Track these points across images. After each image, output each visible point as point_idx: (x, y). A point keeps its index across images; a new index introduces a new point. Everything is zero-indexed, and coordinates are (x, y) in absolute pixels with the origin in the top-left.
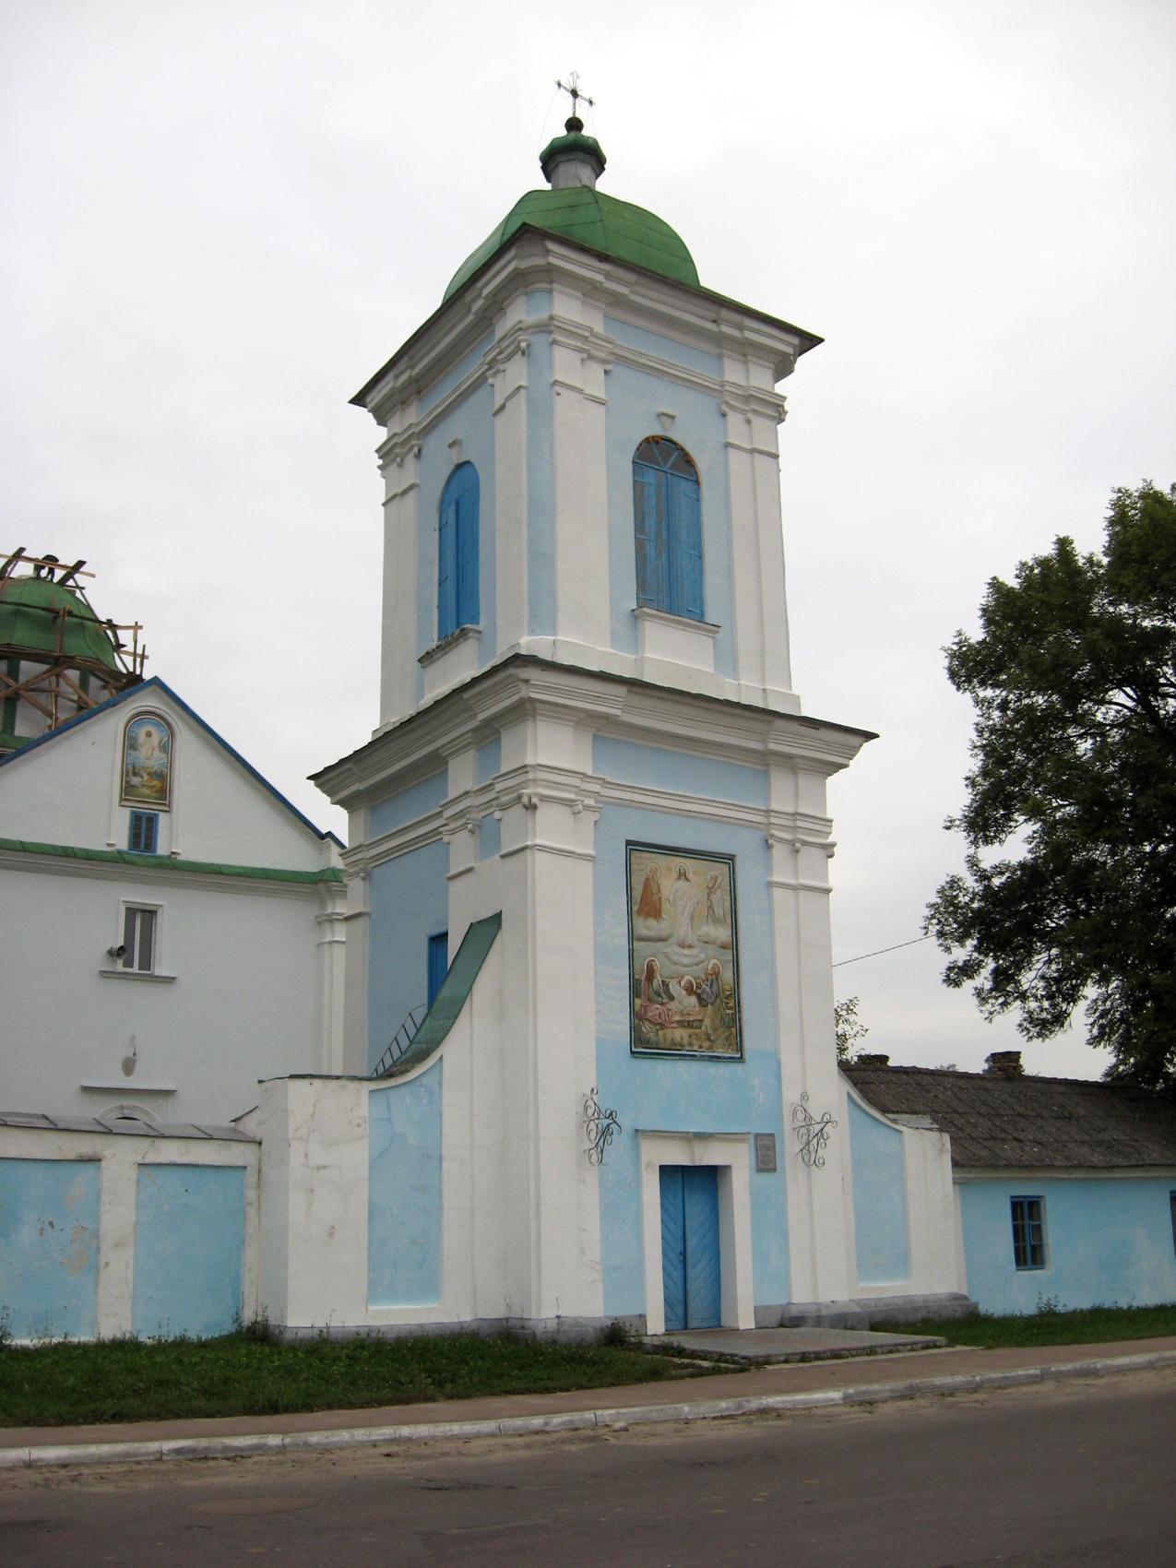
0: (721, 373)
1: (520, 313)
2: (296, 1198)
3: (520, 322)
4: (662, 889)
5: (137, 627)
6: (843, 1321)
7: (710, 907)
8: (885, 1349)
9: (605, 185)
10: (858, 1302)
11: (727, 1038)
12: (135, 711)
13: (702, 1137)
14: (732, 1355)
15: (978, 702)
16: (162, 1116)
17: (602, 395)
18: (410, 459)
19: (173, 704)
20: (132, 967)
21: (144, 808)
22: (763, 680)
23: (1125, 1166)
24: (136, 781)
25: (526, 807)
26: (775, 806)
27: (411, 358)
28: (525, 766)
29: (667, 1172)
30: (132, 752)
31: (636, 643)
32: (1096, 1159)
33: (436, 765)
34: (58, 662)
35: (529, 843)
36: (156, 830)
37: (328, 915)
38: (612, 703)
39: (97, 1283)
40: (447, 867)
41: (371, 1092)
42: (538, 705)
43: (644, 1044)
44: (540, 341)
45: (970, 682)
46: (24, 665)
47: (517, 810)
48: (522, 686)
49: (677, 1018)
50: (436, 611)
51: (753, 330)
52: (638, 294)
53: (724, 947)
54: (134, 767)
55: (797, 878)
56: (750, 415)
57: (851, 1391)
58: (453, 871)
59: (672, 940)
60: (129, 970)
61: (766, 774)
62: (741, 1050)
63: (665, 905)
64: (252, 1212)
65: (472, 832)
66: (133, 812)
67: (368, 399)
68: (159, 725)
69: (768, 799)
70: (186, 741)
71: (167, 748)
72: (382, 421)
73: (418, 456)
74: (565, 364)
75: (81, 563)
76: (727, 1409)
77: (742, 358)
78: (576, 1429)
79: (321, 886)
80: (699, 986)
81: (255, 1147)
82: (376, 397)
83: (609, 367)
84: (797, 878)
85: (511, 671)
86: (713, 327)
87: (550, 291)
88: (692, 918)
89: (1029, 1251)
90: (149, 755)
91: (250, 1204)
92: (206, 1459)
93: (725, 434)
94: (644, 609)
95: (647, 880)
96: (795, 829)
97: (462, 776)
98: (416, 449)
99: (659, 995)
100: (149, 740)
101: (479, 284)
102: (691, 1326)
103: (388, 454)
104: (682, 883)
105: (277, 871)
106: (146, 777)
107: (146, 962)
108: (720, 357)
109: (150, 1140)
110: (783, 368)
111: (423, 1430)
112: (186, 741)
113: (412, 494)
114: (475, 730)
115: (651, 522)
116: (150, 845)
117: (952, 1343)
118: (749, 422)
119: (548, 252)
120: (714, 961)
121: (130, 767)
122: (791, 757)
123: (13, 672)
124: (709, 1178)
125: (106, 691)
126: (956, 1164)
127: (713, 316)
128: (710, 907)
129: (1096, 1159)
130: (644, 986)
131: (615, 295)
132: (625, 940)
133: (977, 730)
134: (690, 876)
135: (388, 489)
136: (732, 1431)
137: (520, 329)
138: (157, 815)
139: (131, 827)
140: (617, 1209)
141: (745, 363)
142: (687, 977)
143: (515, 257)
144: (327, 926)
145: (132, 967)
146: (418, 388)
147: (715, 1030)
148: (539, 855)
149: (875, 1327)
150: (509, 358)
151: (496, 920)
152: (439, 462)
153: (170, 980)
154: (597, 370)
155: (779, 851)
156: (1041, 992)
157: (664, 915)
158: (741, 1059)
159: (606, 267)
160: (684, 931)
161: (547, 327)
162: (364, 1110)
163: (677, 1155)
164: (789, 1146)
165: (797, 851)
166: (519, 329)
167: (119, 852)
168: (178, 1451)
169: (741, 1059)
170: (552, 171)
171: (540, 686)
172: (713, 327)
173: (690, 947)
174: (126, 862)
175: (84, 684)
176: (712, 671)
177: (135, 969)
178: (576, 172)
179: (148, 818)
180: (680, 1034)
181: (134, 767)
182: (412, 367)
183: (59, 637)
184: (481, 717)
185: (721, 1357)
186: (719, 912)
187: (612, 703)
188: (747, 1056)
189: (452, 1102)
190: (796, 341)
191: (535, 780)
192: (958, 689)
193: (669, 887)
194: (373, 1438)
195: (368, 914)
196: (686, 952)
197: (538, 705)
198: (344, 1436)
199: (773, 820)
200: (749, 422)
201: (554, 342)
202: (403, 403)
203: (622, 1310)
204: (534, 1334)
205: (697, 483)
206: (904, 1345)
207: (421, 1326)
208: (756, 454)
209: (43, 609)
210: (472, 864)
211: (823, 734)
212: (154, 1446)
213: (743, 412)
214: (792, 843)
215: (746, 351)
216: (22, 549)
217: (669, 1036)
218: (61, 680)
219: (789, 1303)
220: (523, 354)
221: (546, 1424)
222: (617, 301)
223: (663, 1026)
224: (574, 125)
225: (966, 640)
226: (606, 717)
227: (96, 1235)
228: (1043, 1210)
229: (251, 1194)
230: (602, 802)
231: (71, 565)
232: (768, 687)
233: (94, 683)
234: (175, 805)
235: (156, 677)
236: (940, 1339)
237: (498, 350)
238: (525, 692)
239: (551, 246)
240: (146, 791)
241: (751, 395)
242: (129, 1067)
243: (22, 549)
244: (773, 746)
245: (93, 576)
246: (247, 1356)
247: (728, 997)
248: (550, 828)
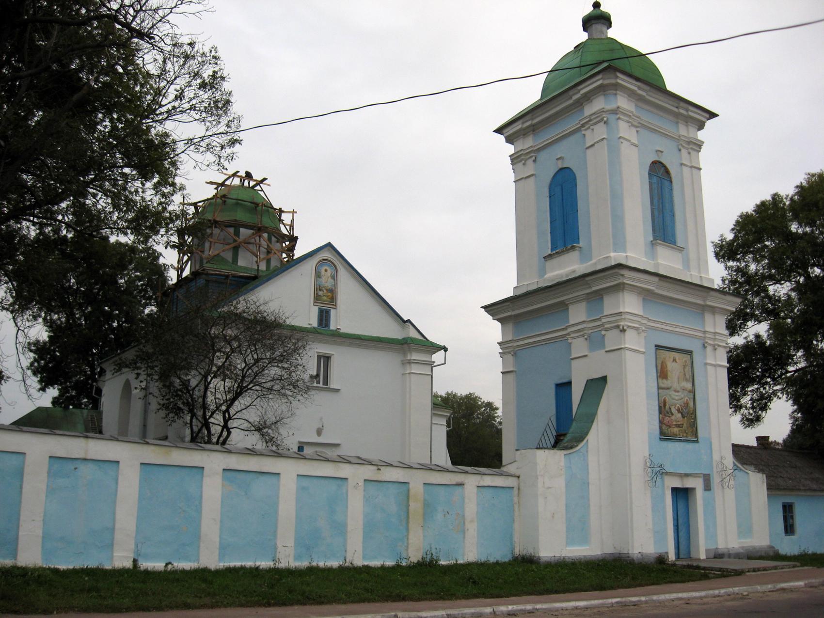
0: (678, 130)
1: (598, 104)
2: (541, 500)
3: (603, 108)
4: (668, 366)
5: (294, 212)
6: (738, 556)
7: (685, 374)
8: (780, 567)
9: (611, 33)
10: (743, 548)
11: (692, 432)
12: (320, 259)
13: (687, 475)
14: (727, 569)
15: (726, 268)
16: (330, 453)
17: (636, 142)
18: (530, 161)
19: (337, 256)
20: (319, 384)
21: (325, 307)
22: (699, 272)
24: (320, 293)
25: (621, 331)
26: (707, 329)
27: (533, 115)
28: (621, 313)
30: (318, 279)
31: (653, 255)
32: (815, 487)
33: (563, 307)
34: (259, 230)
35: (623, 346)
36: (330, 317)
37: (409, 360)
38: (651, 284)
39: (464, 538)
40: (570, 354)
41: (565, 455)
42: (626, 286)
43: (665, 435)
44: (612, 118)
45: (724, 258)
46: (242, 230)
47: (616, 332)
48: (620, 277)
49: (674, 423)
50: (549, 235)
51: (692, 111)
53: (690, 392)
54: (320, 287)
55: (716, 361)
56: (690, 150)
57: (807, 582)
58: (572, 357)
59: (672, 388)
60: (318, 385)
61: (703, 314)
62: (697, 437)
63: (669, 374)
64: (516, 507)
65: (586, 339)
66: (319, 308)
67: (505, 131)
68: (329, 266)
69: (704, 327)
70: (343, 275)
71: (334, 277)
72: (509, 140)
73: (535, 161)
74: (624, 129)
75: (265, 179)
76: (771, 588)
77: (685, 123)
78: (729, 595)
79: (405, 346)
80: (682, 409)
81: (516, 479)
82: (510, 131)
84: (716, 361)
85: (616, 270)
86: (676, 110)
87: (616, 94)
88: (678, 378)
89: (789, 529)
90: (326, 281)
91: (516, 503)
92: (625, 605)
93: (681, 159)
94: (658, 241)
95: (662, 362)
96: (715, 339)
97: (578, 314)
98: (534, 158)
99: (668, 413)
101: (579, 88)
102: (681, 557)
103: (515, 159)
104: (674, 363)
105: (384, 338)
106: (325, 291)
107: (326, 382)
108: (677, 123)
109: (480, 476)
110: (701, 126)
111: (662, 597)
112: (343, 275)
113: (532, 178)
114: (588, 294)
115: (655, 202)
116: (327, 325)
117: (802, 565)
118: (689, 153)
119: (617, 77)
120: (687, 398)
121: (318, 286)
122: (713, 307)
123: (237, 233)
125: (278, 244)
126: (769, 488)
127: (677, 105)
128: (685, 374)
129: (815, 487)
130: (663, 410)
131: (639, 95)
132: (656, 390)
133: (722, 280)
134: (677, 360)
135: (515, 177)
136: (775, 596)
137: (603, 111)
138: (330, 310)
139: (318, 316)
140: (657, 507)
141: (687, 126)
142: (678, 405)
143: (601, 79)
144: (408, 365)
145: (319, 384)
146: (533, 130)
147: (688, 428)
148: (627, 352)
149: (750, 558)
150: (596, 123)
151: (604, 379)
152: (548, 166)
153: (337, 390)
154: (634, 130)
155: (709, 349)
156: (749, 406)
157: (669, 378)
158: (697, 441)
159: (639, 84)
160: (675, 386)
161: (616, 111)
162: (562, 464)
163: (678, 484)
164: (716, 480)
165: (715, 349)
166: (602, 111)
167: (314, 328)
168: (617, 603)
169: (697, 441)
170: (588, 27)
171: (629, 278)
172: (676, 110)
173: (678, 392)
174: (318, 333)
175: (270, 239)
176: (681, 268)
177: (321, 385)
178: (597, 27)
179: (326, 311)
181: (320, 287)
182: (532, 119)
183: (259, 217)
184: (594, 289)
185: (720, 570)
186: (688, 376)
187: (651, 284)
188: (700, 440)
189: (592, 459)
190: (707, 116)
191: (625, 319)
192: (719, 261)
193: (670, 365)
194: (672, 598)
195: (515, 371)
196: (677, 394)
197: (626, 286)
198: (662, 597)
199: (707, 335)
200: (689, 153)
201: (619, 118)
202: (524, 135)
203: (661, 550)
204: (633, 560)
205: (671, 182)
206: (786, 566)
207: (584, 556)
208: (693, 169)
209: (251, 203)
210: (586, 354)
212: (610, 601)
213: (687, 149)
214: (714, 346)
215: (688, 120)
216: (238, 172)
217: (672, 431)
218: (261, 239)
219: (717, 548)
220: (605, 123)
221: (720, 593)
222: (640, 99)
223: (670, 427)
225: (725, 239)
226: (648, 290)
227: (464, 516)
228: (794, 509)
229: (516, 499)
230: (647, 328)
231: (260, 180)
232: (702, 275)
233: (274, 239)
234: (338, 306)
235: (330, 243)
236: (798, 564)
237: (589, 119)
238: (621, 280)
239: (619, 75)
240: (325, 298)
241: (691, 142)
242: (319, 432)
243: (238, 172)
244: (708, 303)
245: (269, 185)
246: (123, 576)
247: (691, 414)
248: (631, 340)
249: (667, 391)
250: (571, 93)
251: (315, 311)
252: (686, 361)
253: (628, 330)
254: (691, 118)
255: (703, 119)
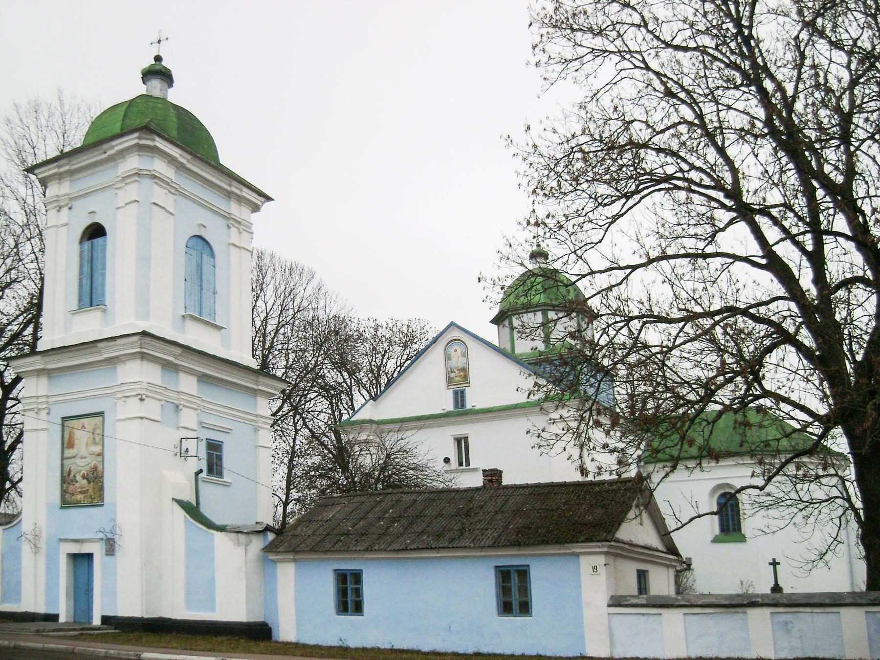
21: (458, 388)
23: (423, 548)
24: (452, 375)
29: (69, 555)
43: (66, 503)
49: (79, 490)
52: (74, 164)
59: (78, 456)
63: (76, 442)
71: (465, 355)
83: (70, 205)
88: (87, 445)
90: (457, 362)
100: (456, 351)
106: (457, 372)
107: (468, 464)
110: (256, 208)
116: (463, 406)
124: (89, 557)
127: (102, 151)
130: (66, 479)
131: (181, 164)
163: (75, 549)
172: (105, 156)
173: (85, 458)
180: (80, 497)
196: (83, 460)
200: (240, 233)
211: (119, 341)
222: (72, 173)
224: (158, 59)
240: (458, 379)
249: (73, 460)
250: (105, 146)
251: (450, 394)
252: (96, 425)
253: (147, 399)
254: (245, 198)
255: (260, 203)
